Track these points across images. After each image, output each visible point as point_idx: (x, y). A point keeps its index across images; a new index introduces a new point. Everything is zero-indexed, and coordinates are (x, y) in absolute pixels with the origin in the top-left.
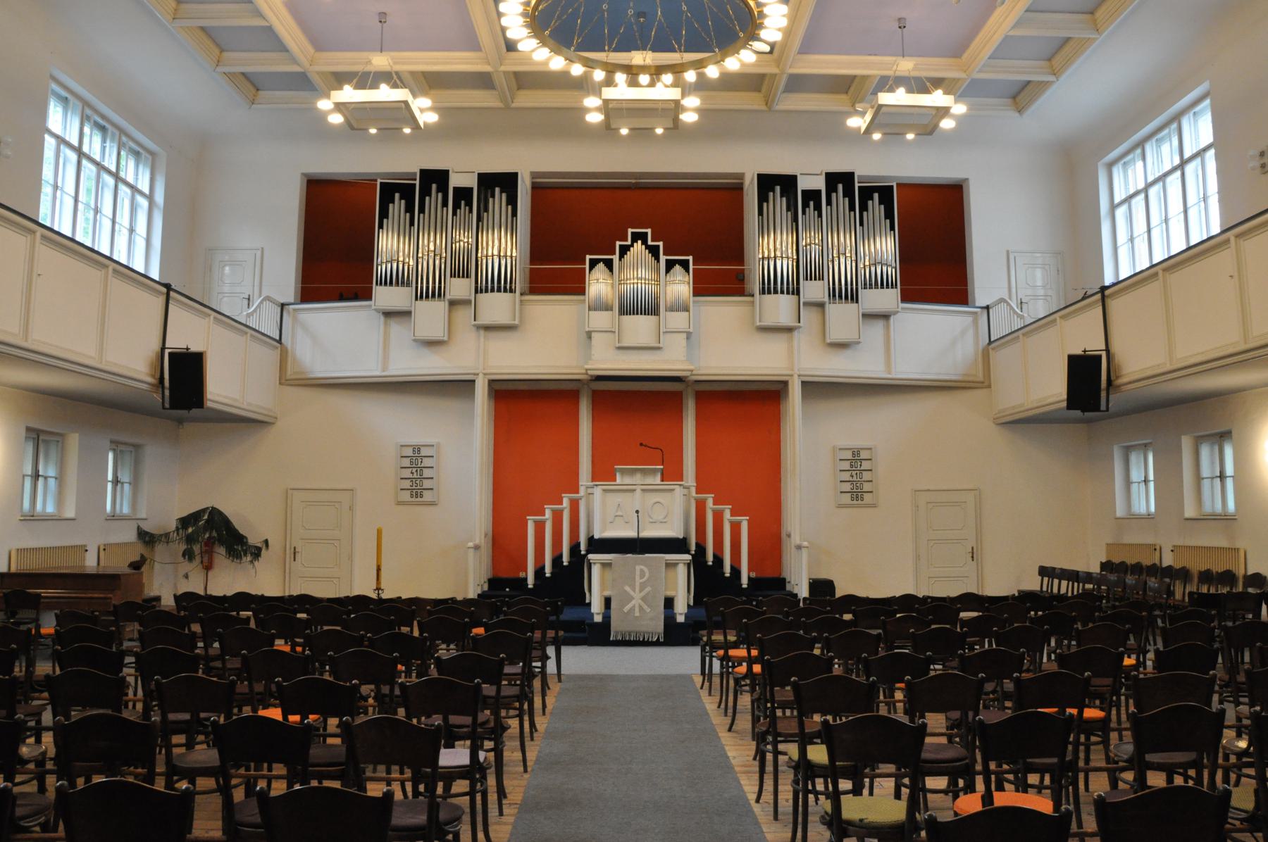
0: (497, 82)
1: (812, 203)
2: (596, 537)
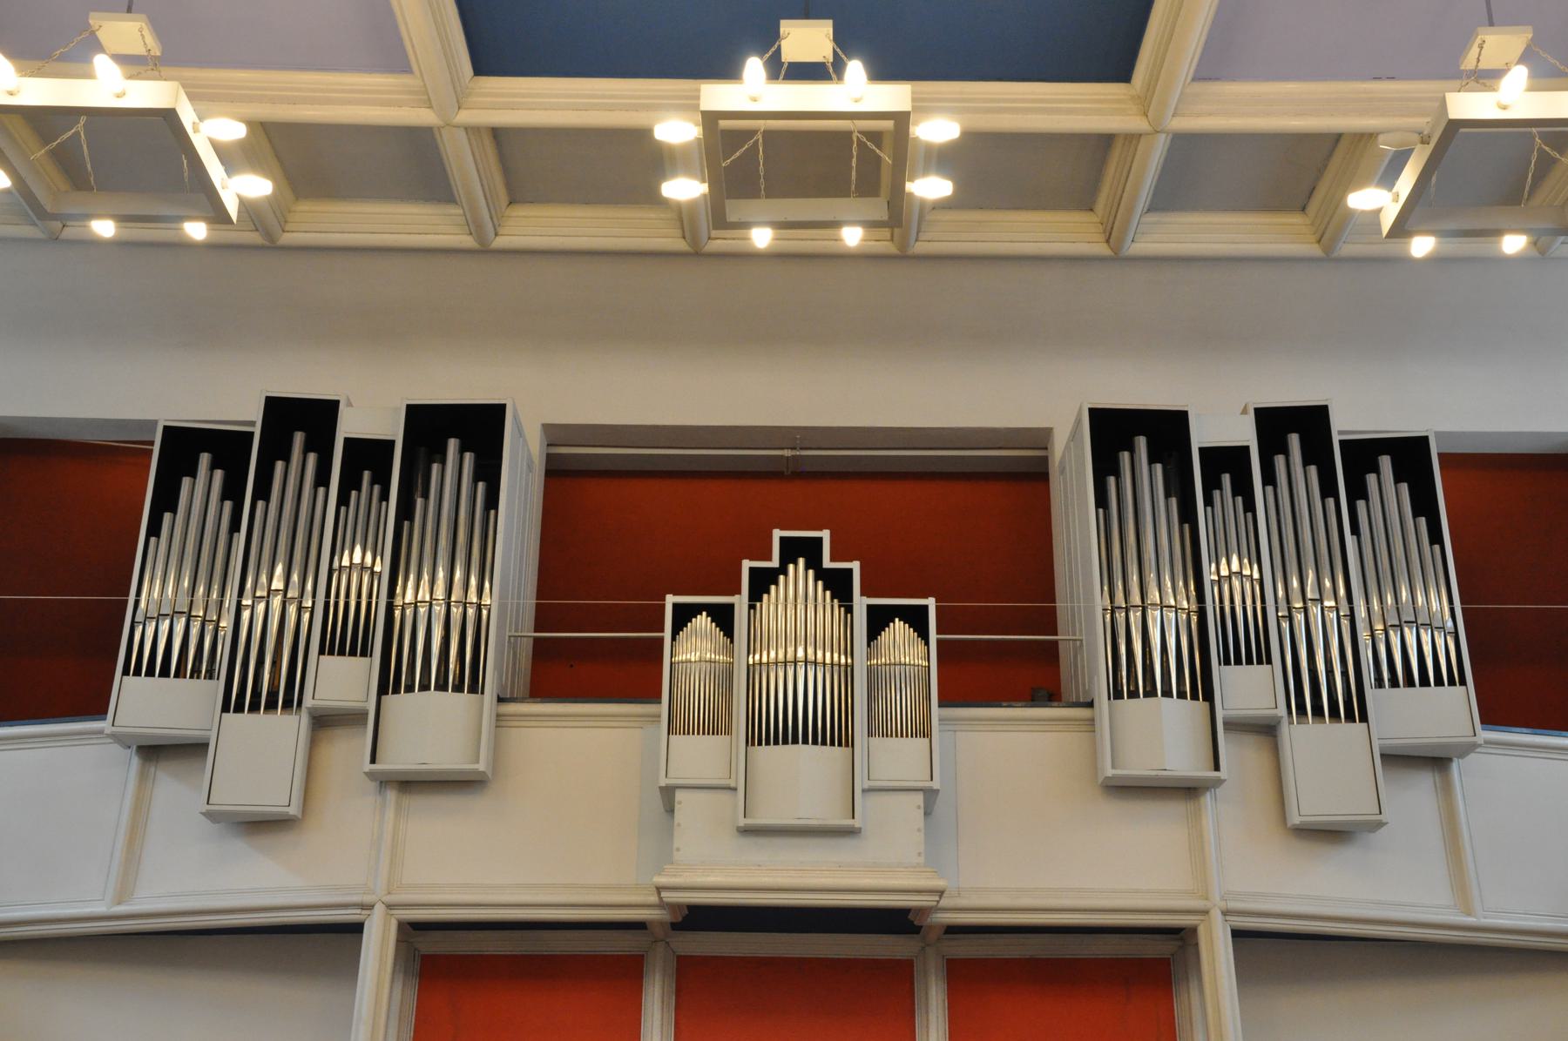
0: (459, 191)
1: (1226, 479)
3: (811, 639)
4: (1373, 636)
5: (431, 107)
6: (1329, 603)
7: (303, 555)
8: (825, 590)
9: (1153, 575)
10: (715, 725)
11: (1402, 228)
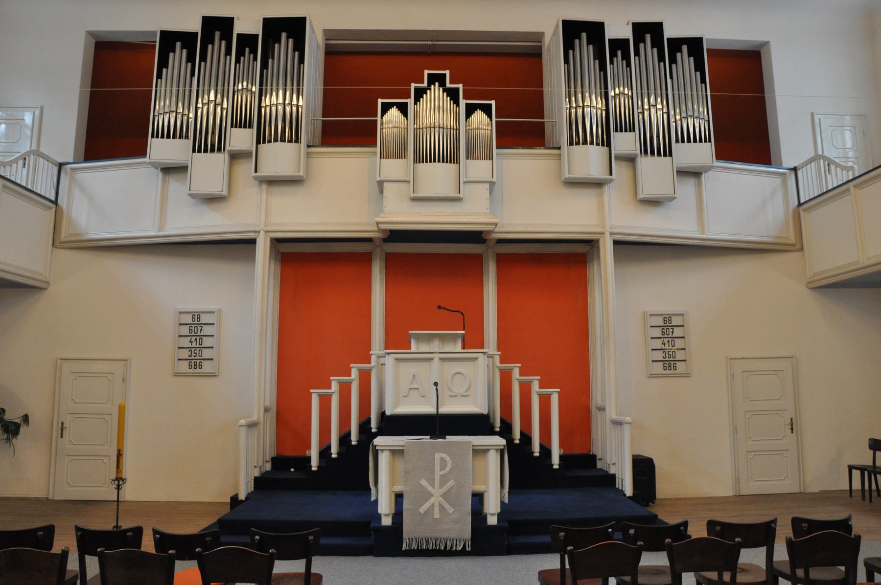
1: (619, 53)
2: (388, 413)
6: (659, 106)
7: (222, 85)
10: (400, 153)
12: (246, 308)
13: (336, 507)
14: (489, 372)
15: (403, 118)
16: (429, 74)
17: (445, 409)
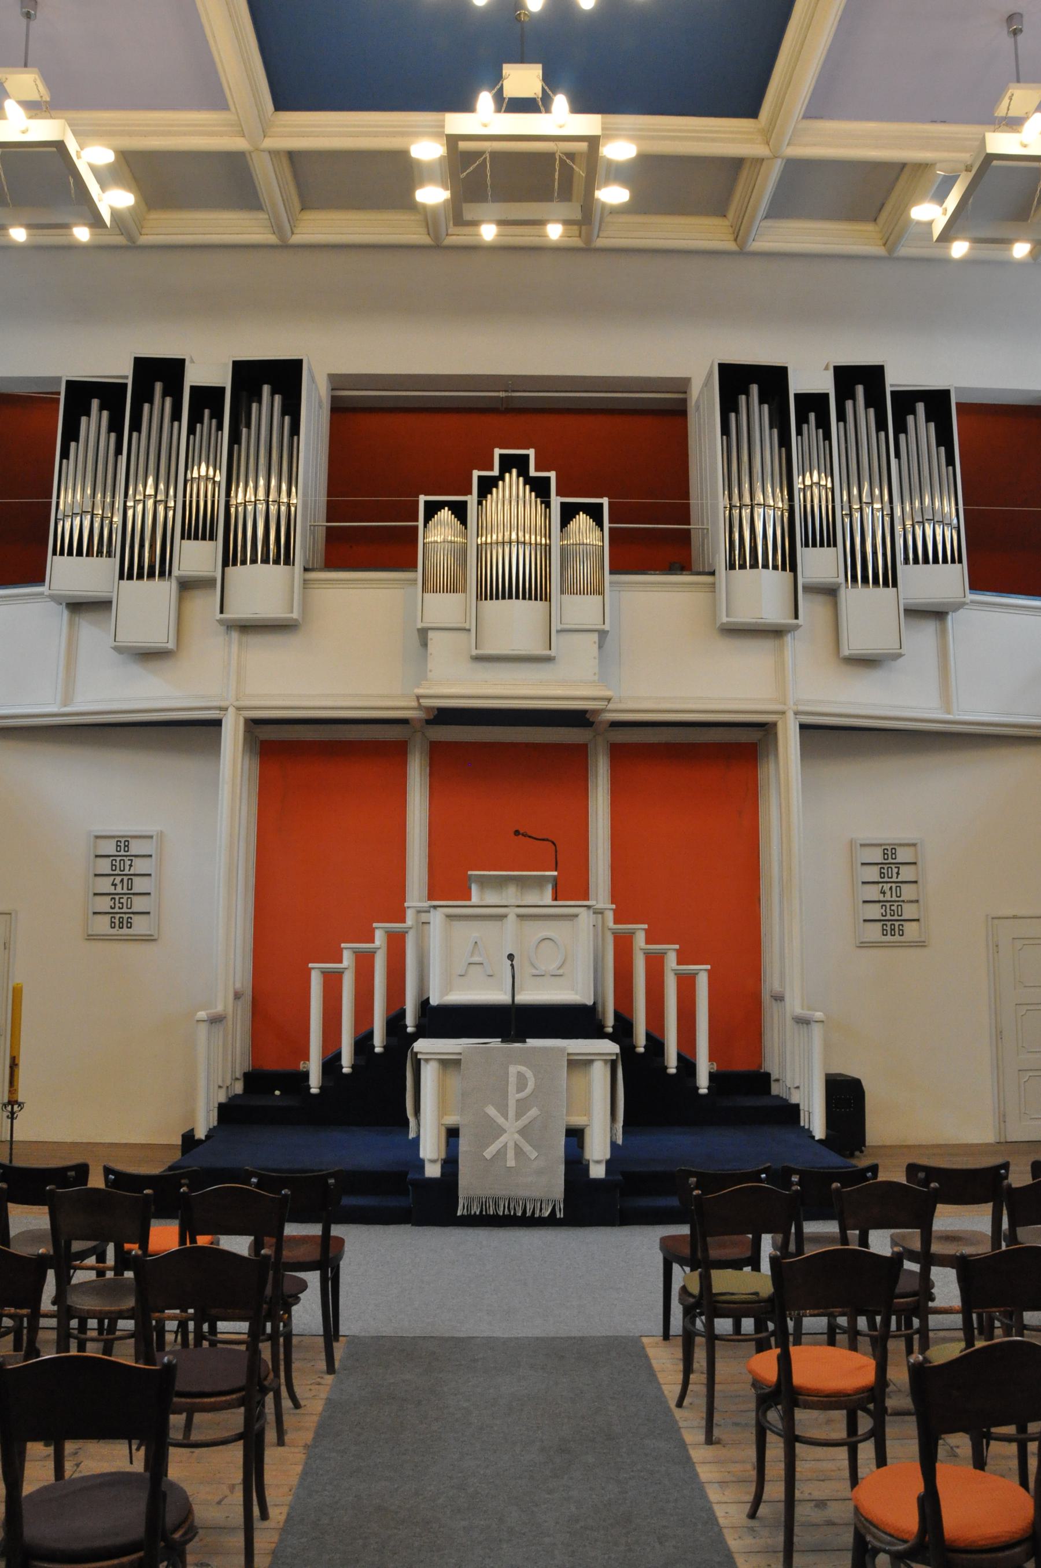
1: (812, 416)
2: (434, 1001)
3: (521, 527)
4: (904, 529)
5: (244, 136)
7: (167, 472)
8: (531, 491)
9: (759, 484)
11: (947, 235)
12: (203, 835)
13: (355, 1150)
14: (596, 936)
15: (457, 523)
16: (501, 456)
17: (524, 997)
